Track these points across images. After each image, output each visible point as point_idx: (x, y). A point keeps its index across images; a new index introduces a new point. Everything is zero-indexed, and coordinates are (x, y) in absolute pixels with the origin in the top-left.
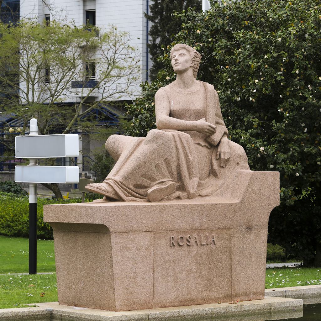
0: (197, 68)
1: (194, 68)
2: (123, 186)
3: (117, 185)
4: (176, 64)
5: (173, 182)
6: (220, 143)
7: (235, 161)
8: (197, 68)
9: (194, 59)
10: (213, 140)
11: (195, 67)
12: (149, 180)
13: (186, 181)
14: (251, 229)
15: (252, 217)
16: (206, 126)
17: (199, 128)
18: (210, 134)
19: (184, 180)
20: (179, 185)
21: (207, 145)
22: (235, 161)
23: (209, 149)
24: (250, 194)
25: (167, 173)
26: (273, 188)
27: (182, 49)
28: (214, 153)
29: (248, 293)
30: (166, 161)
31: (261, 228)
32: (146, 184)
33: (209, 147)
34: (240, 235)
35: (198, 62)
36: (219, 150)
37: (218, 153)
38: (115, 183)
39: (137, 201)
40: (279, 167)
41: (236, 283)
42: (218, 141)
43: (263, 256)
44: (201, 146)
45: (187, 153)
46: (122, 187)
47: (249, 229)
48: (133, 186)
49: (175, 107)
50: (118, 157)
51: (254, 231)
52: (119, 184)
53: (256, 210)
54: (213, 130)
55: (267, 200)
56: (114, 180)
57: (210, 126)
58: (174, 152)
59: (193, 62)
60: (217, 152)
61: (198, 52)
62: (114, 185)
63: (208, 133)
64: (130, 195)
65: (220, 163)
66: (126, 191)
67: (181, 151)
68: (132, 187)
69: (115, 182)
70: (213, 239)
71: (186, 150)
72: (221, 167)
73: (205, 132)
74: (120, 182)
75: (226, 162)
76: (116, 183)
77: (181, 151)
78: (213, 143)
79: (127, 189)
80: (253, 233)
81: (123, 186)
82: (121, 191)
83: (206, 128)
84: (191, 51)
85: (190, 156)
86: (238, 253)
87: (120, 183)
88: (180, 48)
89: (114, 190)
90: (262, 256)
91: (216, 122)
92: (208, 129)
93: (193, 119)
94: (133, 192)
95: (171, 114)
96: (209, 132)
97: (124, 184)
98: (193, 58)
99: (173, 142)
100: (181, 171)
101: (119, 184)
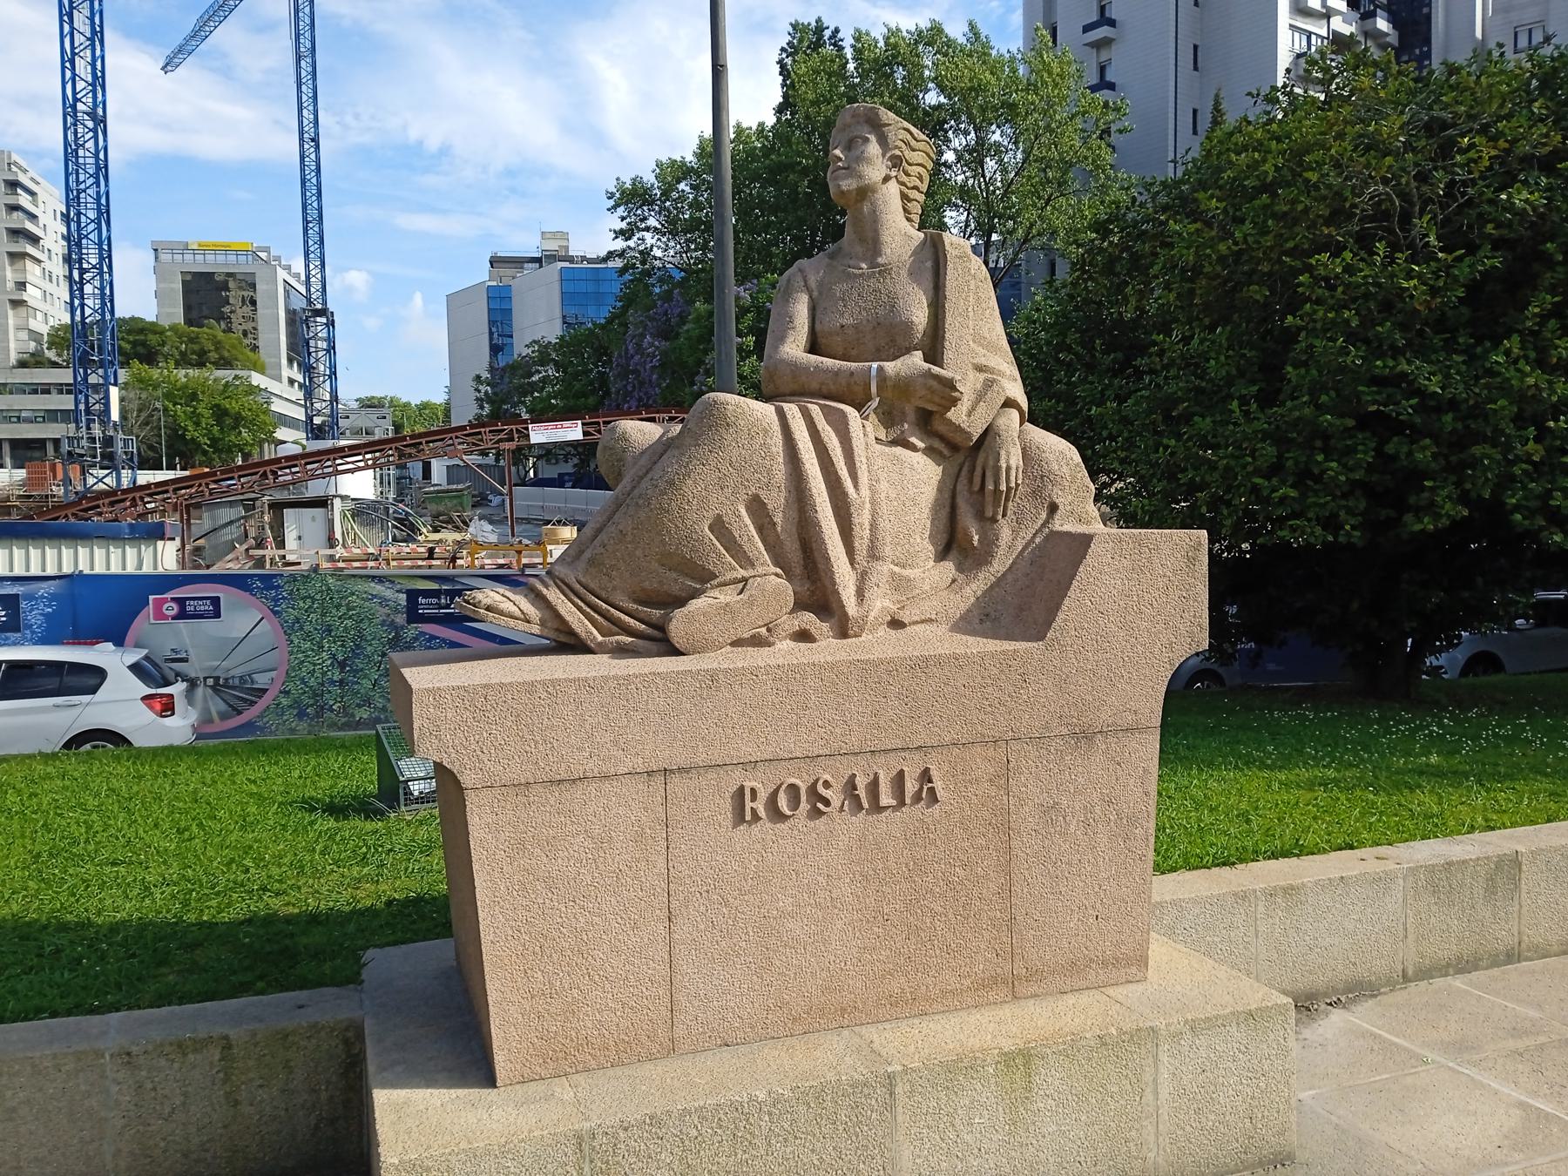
30: (757, 507)
32: (675, 589)
42: (980, 431)
64: (615, 629)
70: (930, 785)
72: (989, 519)
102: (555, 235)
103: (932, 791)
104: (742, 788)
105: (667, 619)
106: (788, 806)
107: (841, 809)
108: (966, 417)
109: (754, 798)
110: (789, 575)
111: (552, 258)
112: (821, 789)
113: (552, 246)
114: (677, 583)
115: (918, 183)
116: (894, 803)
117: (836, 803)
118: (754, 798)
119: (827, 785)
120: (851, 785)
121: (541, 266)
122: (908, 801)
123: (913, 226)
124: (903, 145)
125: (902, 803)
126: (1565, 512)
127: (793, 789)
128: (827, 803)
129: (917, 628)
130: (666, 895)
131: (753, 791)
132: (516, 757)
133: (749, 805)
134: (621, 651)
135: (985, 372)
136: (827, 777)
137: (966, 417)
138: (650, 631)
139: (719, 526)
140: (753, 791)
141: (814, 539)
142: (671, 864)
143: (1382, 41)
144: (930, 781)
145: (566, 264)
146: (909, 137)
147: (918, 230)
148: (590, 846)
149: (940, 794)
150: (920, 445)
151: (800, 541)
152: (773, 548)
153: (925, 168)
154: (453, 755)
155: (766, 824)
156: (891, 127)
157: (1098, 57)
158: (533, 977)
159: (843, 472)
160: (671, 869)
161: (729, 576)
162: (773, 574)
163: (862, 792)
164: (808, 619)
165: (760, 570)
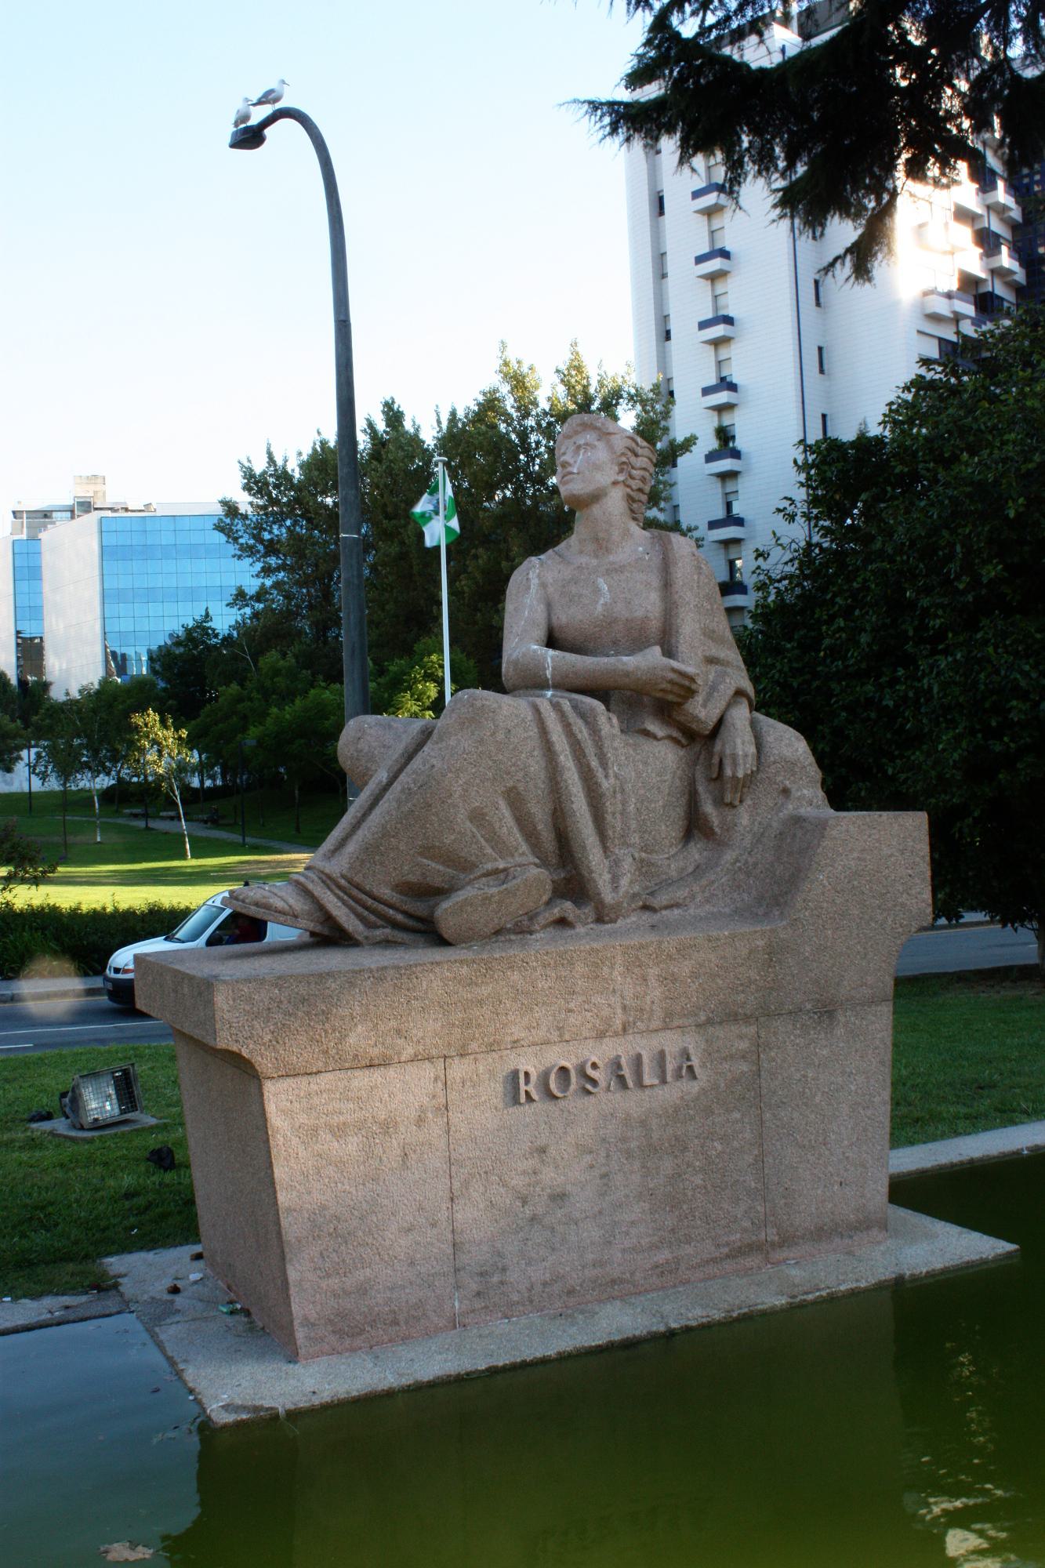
0: (640, 490)
1: (632, 490)
2: (355, 892)
3: (334, 887)
4: (565, 479)
5: (539, 870)
6: (723, 728)
7: (775, 783)
8: (640, 490)
9: (624, 459)
10: (696, 719)
11: (634, 487)
12: (448, 866)
13: (586, 862)
14: (831, 1014)
15: (833, 972)
16: (662, 670)
17: (638, 679)
18: (679, 696)
19: (580, 859)
20: (565, 878)
21: (676, 734)
22: (775, 783)
23: (683, 746)
24: (823, 894)
25: (517, 838)
26: (907, 868)
27: (584, 430)
28: (701, 760)
29: (825, 1228)
30: (515, 799)
31: (869, 1007)
32: (437, 882)
33: (684, 741)
34: (792, 1037)
35: (645, 469)
36: (718, 747)
37: (716, 760)
38: (323, 882)
39: (400, 943)
40: (944, 537)
41: (783, 1201)
42: (715, 720)
43: (877, 1099)
44: (655, 737)
45: (588, 766)
46: (350, 896)
47: (827, 1012)
48: (392, 890)
49: (567, 617)
50: (365, 778)
51: (842, 1019)
52: (340, 887)
53: (848, 948)
54: (687, 683)
55: (884, 910)
56: (322, 872)
57: (674, 670)
58: (536, 766)
59: (621, 471)
60: (711, 754)
61: (639, 440)
62: (319, 891)
63: (671, 692)
64: (380, 922)
65: (722, 792)
66: (367, 908)
67: (566, 760)
68: (386, 892)
69: (324, 878)
70: (689, 1063)
71: (585, 756)
72: (727, 805)
73: (662, 690)
74: (343, 876)
75: (743, 786)
76: (329, 882)
77: (566, 760)
78: (694, 726)
79: (370, 902)
80: (838, 1024)
81: (355, 892)
82: (345, 910)
83: (663, 678)
84: (615, 434)
85: (600, 774)
86: (784, 1100)
87: (343, 882)
88: (579, 429)
89: (321, 908)
90: (875, 1100)
91: (705, 657)
92: (671, 682)
93: (628, 652)
94: (391, 912)
95: (552, 641)
96: (676, 689)
97: (358, 887)
98: (623, 454)
99: (534, 732)
100: (567, 827)
101: (340, 887)
102: (94, 478)
103: (690, 1068)
104: (515, 1074)
105: (433, 909)
106: (558, 1088)
107: (608, 1089)
108: (703, 711)
109: (527, 1082)
110: (544, 863)
111: (86, 506)
112: (590, 1072)
113: (85, 492)
114: (437, 871)
115: (641, 485)
116: (656, 1081)
117: (603, 1084)
118: (527, 1082)
119: (594, 1066)
120: (617, 1065)
121: (73, 517)
122: (669, 1078)
123: (639, 525)
124: (629, 453)
125: (664, 1081)
126: (1, 871)
127: (563, 1070)
128: (594, 1082)
129: (664, 912)
130: (448, 1177)
131: (527, 1074)
132: (308, 1047)
133: (523, 1088)
134: (387, 943)
135: (716, 664)
136: (594, 1059)
137: (703, 711)
138: (411, 923)
139: (478, 817)
140: (527, 1074)
141: (569, 829)
142: (452, 1146)
143: (1009, 279)
144: (688, 1059)
145: (109, 514)
146: (634, 445)
147: (644, 529)
148: (378, 1132)
149: (697, 1070)
150: (660, 733)
151: (556, 830)
152: (531, 835)
153: (648, 471)
154: (251, 1046)
155: (541, 1106)
156: (616, 436)
157: (713, 290)
158: (328, 1257)
159: (594, 763)
160: (452, 1151)
161: (489, 866)
162: (531, 864)
163: (627, 1072)
164: (567, 907)
165: (518, 859)
